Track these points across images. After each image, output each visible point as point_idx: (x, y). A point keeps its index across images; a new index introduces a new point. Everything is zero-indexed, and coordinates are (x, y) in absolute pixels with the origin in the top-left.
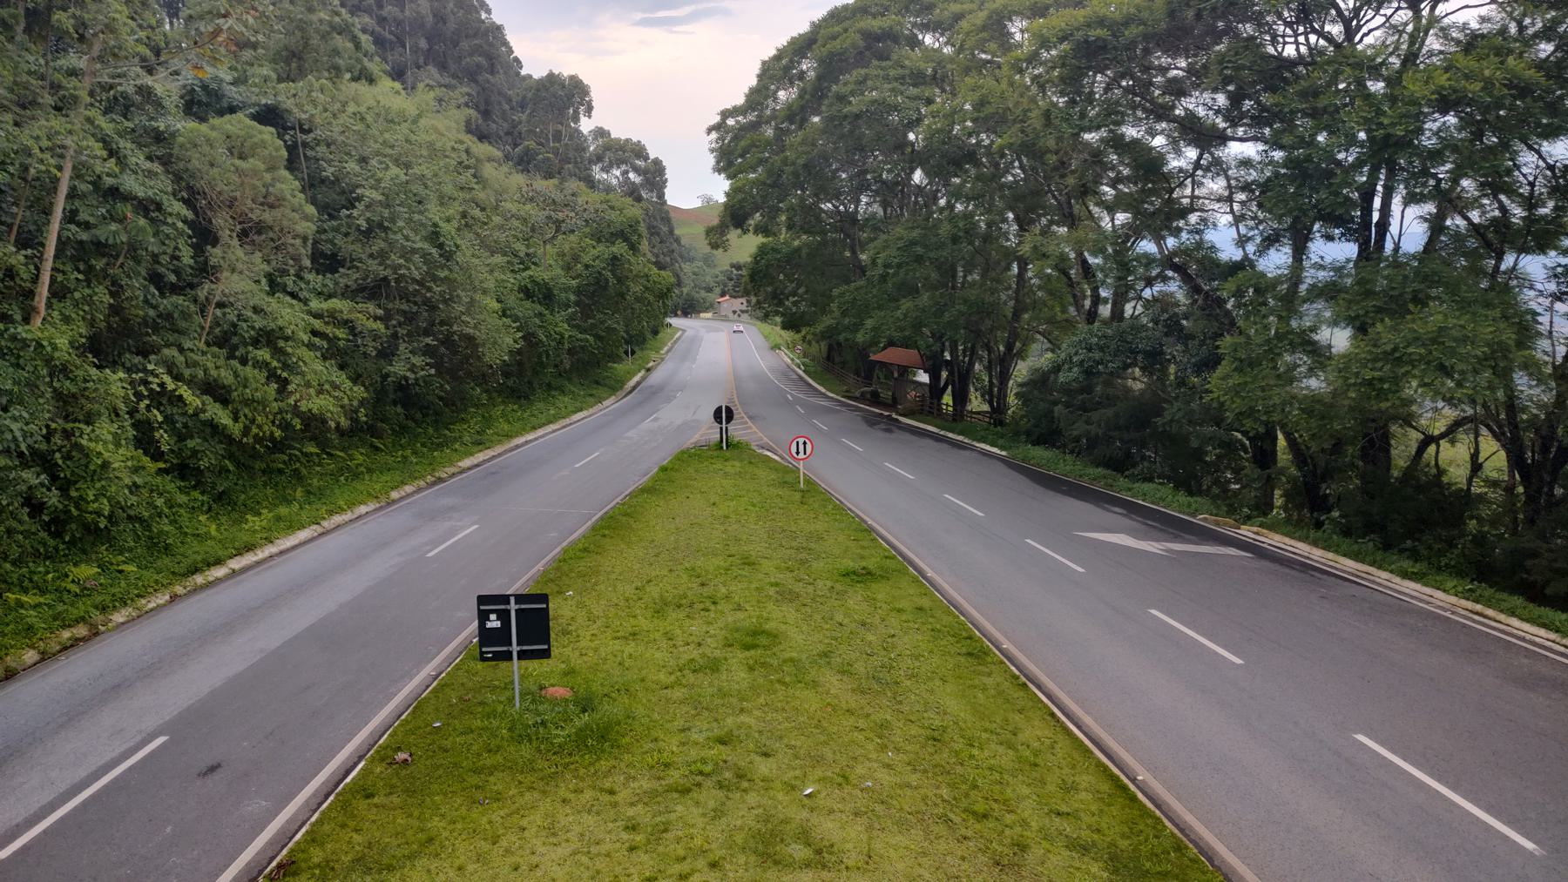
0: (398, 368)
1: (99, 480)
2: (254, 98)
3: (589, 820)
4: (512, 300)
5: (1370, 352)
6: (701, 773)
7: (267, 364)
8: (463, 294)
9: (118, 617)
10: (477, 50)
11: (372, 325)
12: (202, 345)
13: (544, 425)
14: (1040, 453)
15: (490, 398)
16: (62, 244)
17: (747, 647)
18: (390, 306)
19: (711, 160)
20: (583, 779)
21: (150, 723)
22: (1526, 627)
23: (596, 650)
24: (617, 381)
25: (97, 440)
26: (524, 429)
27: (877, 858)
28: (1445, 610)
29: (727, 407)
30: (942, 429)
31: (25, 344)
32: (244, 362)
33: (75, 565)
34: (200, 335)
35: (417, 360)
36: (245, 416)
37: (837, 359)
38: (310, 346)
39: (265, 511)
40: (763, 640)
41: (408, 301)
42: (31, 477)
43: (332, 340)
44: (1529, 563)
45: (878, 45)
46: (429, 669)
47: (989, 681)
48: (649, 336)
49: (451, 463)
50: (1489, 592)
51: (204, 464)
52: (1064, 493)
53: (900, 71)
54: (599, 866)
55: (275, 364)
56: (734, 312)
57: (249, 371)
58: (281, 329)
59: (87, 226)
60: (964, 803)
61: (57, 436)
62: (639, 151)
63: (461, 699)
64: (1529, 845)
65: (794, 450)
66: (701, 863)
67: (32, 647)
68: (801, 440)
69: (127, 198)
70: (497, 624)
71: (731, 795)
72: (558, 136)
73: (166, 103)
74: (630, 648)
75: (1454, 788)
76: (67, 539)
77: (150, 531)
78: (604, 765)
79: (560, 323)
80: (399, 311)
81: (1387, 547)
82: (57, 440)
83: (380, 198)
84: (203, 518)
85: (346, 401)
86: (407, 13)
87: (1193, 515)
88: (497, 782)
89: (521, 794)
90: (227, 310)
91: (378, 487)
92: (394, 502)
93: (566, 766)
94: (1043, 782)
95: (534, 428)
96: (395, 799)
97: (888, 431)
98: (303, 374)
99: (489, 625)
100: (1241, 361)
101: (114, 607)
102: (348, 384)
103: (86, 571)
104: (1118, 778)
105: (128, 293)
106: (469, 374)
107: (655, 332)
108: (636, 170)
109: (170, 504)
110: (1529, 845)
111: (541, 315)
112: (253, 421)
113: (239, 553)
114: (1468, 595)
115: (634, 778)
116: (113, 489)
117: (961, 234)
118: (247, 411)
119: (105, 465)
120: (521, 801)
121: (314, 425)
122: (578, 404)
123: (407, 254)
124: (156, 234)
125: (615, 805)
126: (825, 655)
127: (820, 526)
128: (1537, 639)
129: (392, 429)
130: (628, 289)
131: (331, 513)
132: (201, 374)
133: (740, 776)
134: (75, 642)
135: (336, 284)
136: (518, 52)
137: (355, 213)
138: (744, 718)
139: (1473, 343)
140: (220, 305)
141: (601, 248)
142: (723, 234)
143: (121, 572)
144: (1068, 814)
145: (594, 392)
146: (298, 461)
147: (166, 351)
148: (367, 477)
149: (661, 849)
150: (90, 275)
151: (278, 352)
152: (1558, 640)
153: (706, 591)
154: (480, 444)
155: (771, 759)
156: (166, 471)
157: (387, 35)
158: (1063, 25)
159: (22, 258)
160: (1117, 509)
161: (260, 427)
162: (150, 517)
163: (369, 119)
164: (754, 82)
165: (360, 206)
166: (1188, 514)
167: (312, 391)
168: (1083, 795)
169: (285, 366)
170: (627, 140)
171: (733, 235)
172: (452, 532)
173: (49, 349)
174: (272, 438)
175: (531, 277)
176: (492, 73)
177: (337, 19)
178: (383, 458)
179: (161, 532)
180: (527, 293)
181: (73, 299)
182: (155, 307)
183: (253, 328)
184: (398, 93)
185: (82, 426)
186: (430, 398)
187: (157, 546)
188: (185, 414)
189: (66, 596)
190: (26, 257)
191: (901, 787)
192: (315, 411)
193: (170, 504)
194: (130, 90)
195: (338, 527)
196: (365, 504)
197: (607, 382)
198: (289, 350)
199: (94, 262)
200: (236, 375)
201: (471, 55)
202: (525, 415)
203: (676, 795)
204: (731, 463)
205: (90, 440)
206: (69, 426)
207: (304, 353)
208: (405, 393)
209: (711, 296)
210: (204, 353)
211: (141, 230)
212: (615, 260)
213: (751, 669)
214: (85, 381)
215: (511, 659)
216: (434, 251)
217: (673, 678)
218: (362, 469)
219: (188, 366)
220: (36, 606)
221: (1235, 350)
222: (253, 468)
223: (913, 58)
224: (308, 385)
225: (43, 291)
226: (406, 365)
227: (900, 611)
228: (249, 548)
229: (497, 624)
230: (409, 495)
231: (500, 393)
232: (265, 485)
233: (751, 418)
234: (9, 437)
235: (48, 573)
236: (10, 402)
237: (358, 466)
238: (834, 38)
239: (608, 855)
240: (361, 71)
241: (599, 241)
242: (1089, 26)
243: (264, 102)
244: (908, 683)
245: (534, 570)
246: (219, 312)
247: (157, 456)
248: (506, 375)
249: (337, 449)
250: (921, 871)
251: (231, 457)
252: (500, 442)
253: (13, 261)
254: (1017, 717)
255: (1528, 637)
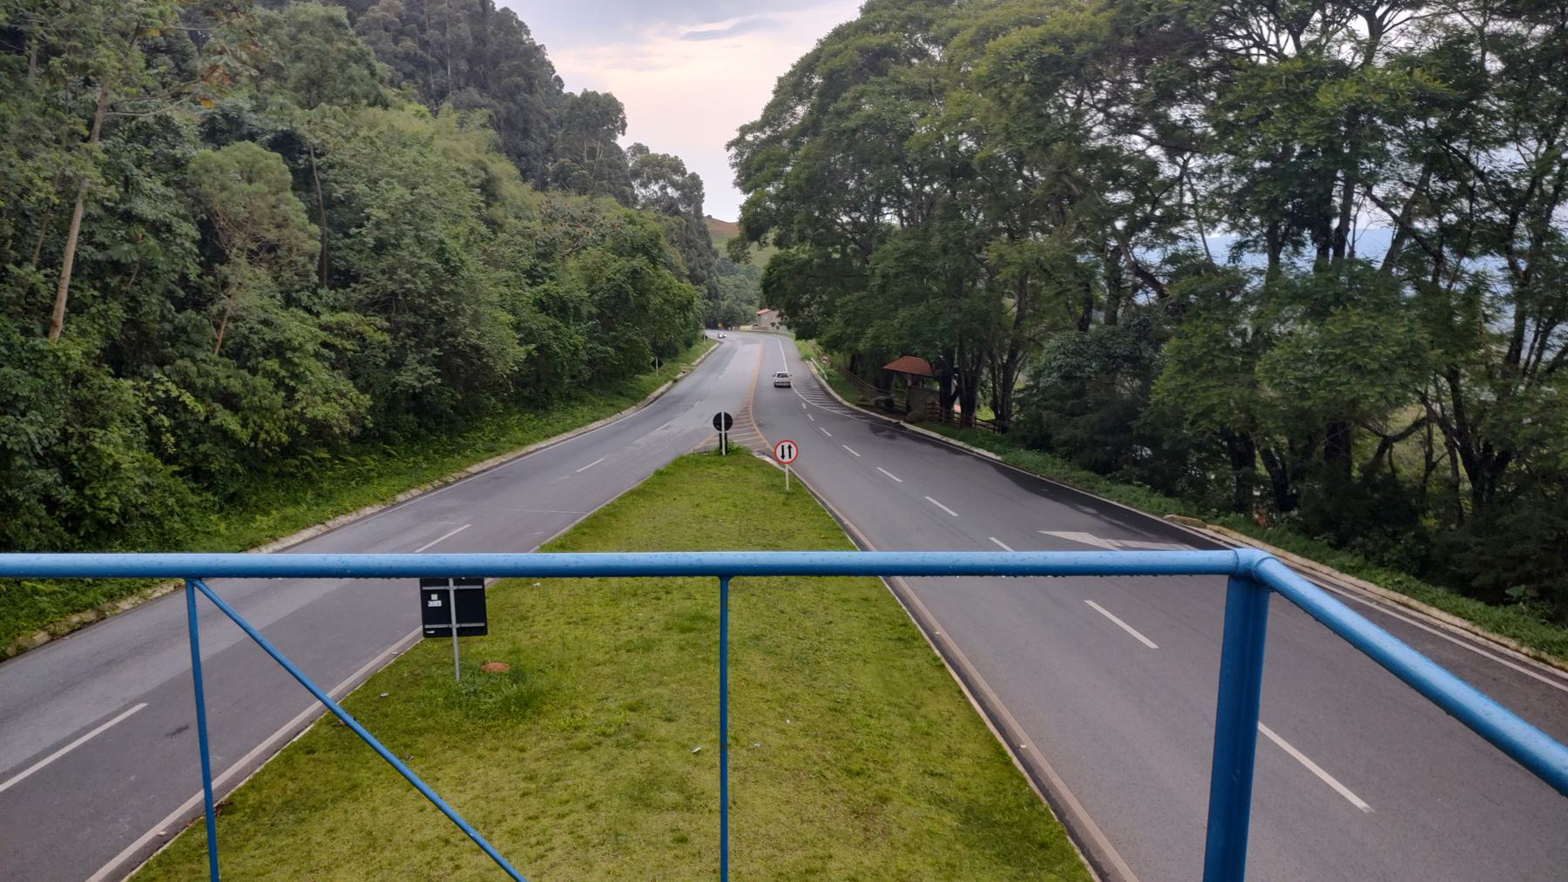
0: (407, 378)
1: (111, 480)
2: (272, 125)
3: (496, 772)
4: (526, 314)
5: (1292, 353)
6: (604, 734)
7: (277, 374)
9: (125, 605)
10: (516, 71)
11: (379, 336)
12: (215, 357)
13: (559, 433)
14: (1030, 457)
15: (506, 408)
16: (78, 265)
17: (684, 631)
18: (399, 318)
19: (732, 174)
20: (500, 740)
21: (136, 691)
22: (1444, 616)
23: (546, 633)
24: (641, 392)
25: (108, 443)
27: (740, 804)
28: (1371, 600)
30: (945, 435)
31: (42, 355)
35: (424, 370)
36: (254, 422)
37: (859, 369)
38: (317, 355)
41: (416, 314)
42: (49, 477)
43: (340, 352)
44: (1456, 556)
45: (877, 61)
46: (392, 649)
47: (910, 663)
48: (682, 348)
49: (461, 469)
50: (1415, 583)
51: (214, 467)
52: (1045, 495)
53: (896, 87)
55: (283, 373)
56: (773, 324)
57: (259, 380)
58: (289, 340)
59: (101, 247)
60: (844, 763)
61: (75, 439)
62: (676, 166)
64: (1360, 804)
65: (794, 451)
67: (43, 628)
68: (786, 445)
69: (142, 221)
70: (438, 603)
71: (625, 752)
72: (592, 153)
73: (184, 131)
75: (1311, 758)
76: (82, 533)
77: (163, 528)
79: (576, 335)
80: (408, 325)
81: (1340, 544)
82: (74, 443)
83: (386, 216)
84: (214, 517)
85: (352, 408)
86: (448, 36)
87: (1161, 515)
88: (422, 743)
89: (444, 752)
90: (240, 324)
91: (384, 490)
93: (488, 729)
94: (929, 748)
95: (548, 436)
96: (333, 755)
97: (891, 437)
98: (309, 383)
99: (431, 604)
100: (1185, 363)
101: (122, 595)
104: (1000, 745)
107: (689, 345)
108: (674, 185)
109: (182, 503)
110: (1360, 804)
111: (555, 327)
114: (1397, 587)
116: (124, 488)
117: (951, 245)
118: (255, 417)
119: (116, 466)
121: (320, 430)
122: (595, 414)
123: (413, 270)
124: (166, 251)
125: (522, 760)
126: (757, 638)
127: (793, 526)
128: (1452, 628)
129: (404, 437)
130: (648, 300)
131: (336, 514)
132: (212, 383)
133: (639, 737)
134: (84, 625)
136: (560, 71)
137: (364, 231)
139: (1384, 343)
140: (234, 319)
141: (623, 261)
142: (744, 247)
144: (941, 775)
145: (615, 402)
146: (310, 465)
147: (179, 362)
148: (376, 482)
150: (106, 293)
151: (286, 362)
152: (1470, 627)
154: (491, 451)
156: (181, 474)
157: (430, 58)
158: (1020, 42)
159: (40, 276)
160: (1089, 510)
161: (267, 432)
162: (162, 515)
163: (379, 143)
164: (770, 97)
165: (369, 225)
166: (1156, 514)
167: (318, 399)
168: (964, 760)
169: (294, 376)
170: (664, 156)
171: (753, 247)
172: (445, 530)
173: (64, 359)
174: (280, 444)
175: (545, 290)
176: (531, 92)
177: (353, 48)
178: (394, 464)
180: (542, 306)
182: (171, 322)
183: (264, 340)
184: (423, 116)
185: (96, 430)
188: (197, 420)
189: (79, 586)
190: (46, 275)
191: (787, 748)
192: (320, 417)
193: (182, 503)
194: (151, 120)
195: (344, 525)
196: (371, 506)
197: (630, 392)
198: (296, 360)
199: (108, 280)
200: (245, 384)
201: (510, 76)
203: (576, 752)
204: (727, 467)
207: (314, 364)
208: (418, 401)
209: (753, 309)
210: (216, 364)
211: (150, 249)
212: (635, 274)
213: (682, 649)
214: (101, 388)
215: (451, 635)
216: (439, 266)
217: (608, 656)
218: (373, 474)
219: (200, 375)
221: (1179, 353)
222: (265, 472)
223: (915, 69)
224: (314, 393)
225: (61, 306)
226: (415, 374)
227: (846, 601)
229: (438, 603)
230: (414, 498)
231: (516, 402)
232: (277, 488)
233: (760, 425)
234: (25, 439)
236: (28, 408)
237: (369, 471)
238: (835, 55)
239: (503, 800)
240: (376, 97)
241: (621, 255)
242: (1044, 43)
243: (280, 128)
244: (828, 663)
246: (231, 326)
247: (169, 460)
248: (517, 384)
249: (349, 454)
250: (780, 815)
251: (243, 461)
252: (511, 449)
253: (32, 280)
254: (926, 694)
255: (1443, 625)
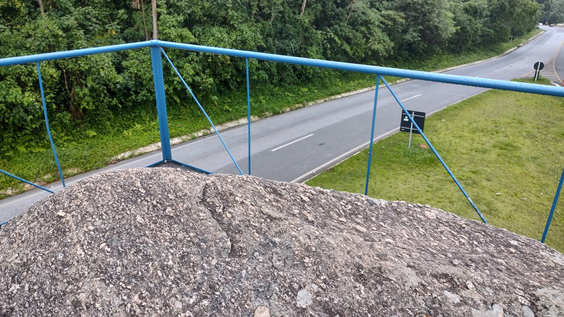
0: (408, 37)
3: (418, 181)
8: (436, 10)
9: (310, 104)
12: (346, 25)
13: (462, 64)
15: (443, 52)
17: (501, 149)
18: (409, 14)
20: (421, 171)
23: (444, 138)
24: (501, 50)
25: (312, 51)
26: (453, 65)
29: (541, 63)
31: (297, 21)
32: (357, 31)
33: (303, 87)
34: (346, 21)
38: (379, 26)
39: (356, 81)
40: (509, 148)
43: (386, 25)
54: (415, 192)
55: (366, 32)
57: (358, 34)
58: (370, 20)
63: (393, 142)
66: (447, 201)
74: (457, 140)
78: (430, 169)
85: (387, 47)
88: (394, 166)
89: (401, 170)
92: (398, 83)
95: (457, 65)
99: (405, 120)
102: (389, 41)
103: (305, 90)
105: (327, 7)
106: (436, 42)
107: (529, 31)
111: (470, 20)
112: (356, 51)
113: (346, 92)
115: (438, 175)
118: (355, 47)
120: (400, 172)
122: (479, 58)
125: (428, 180)
130: (515, 10)
132: (344, 34)
133: (474, 183)
134: (300, 108)
135: (392, 5)
138: (486, 168)
140: (353, 11)
143: (313, 92)
145: (489, 54)
147: (335, 26)
149: (436, 194)
151: (368, 28)
153: (497, 129)
155: (490, 182)
161: (358, 53)
167: (376, 42)
169: (370, 33)
172: (412, 95)
175: (469, 4)
179: (326, 82)
181: (311, 8)
182: (334, 11)
183: (362, 19)
186: (419, 49)
187: (324, 86)
189: (299, 96)
192: (376, 49)
198: (371, 28)
200: (354, 35)
202: (455, 60)
203: (448, 182)
205: (310, 51)
206: (306, 47)
207: (377, 29)
214: (312, 33)
215: (410, 132)
217: (467, 152)
219: (340, 31)
220: (292, 97)
224: (375, 40)
225: (304, 5)
226: (412, 36)
228: (349, 91)
231: (447, 50)
235: (296, 88)
236: (292, 38)
239: (419, 191)
245: (435, 111)
246: (352, 14)
